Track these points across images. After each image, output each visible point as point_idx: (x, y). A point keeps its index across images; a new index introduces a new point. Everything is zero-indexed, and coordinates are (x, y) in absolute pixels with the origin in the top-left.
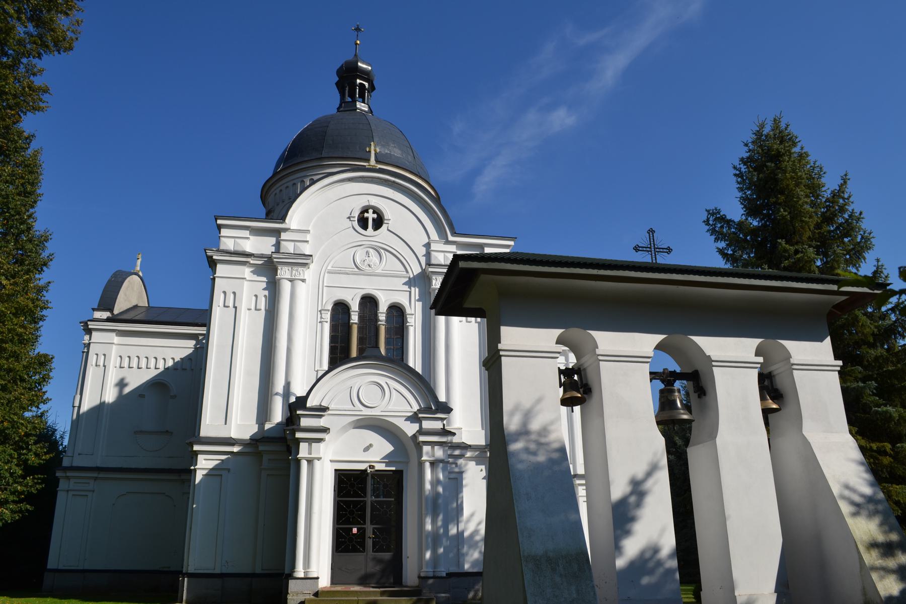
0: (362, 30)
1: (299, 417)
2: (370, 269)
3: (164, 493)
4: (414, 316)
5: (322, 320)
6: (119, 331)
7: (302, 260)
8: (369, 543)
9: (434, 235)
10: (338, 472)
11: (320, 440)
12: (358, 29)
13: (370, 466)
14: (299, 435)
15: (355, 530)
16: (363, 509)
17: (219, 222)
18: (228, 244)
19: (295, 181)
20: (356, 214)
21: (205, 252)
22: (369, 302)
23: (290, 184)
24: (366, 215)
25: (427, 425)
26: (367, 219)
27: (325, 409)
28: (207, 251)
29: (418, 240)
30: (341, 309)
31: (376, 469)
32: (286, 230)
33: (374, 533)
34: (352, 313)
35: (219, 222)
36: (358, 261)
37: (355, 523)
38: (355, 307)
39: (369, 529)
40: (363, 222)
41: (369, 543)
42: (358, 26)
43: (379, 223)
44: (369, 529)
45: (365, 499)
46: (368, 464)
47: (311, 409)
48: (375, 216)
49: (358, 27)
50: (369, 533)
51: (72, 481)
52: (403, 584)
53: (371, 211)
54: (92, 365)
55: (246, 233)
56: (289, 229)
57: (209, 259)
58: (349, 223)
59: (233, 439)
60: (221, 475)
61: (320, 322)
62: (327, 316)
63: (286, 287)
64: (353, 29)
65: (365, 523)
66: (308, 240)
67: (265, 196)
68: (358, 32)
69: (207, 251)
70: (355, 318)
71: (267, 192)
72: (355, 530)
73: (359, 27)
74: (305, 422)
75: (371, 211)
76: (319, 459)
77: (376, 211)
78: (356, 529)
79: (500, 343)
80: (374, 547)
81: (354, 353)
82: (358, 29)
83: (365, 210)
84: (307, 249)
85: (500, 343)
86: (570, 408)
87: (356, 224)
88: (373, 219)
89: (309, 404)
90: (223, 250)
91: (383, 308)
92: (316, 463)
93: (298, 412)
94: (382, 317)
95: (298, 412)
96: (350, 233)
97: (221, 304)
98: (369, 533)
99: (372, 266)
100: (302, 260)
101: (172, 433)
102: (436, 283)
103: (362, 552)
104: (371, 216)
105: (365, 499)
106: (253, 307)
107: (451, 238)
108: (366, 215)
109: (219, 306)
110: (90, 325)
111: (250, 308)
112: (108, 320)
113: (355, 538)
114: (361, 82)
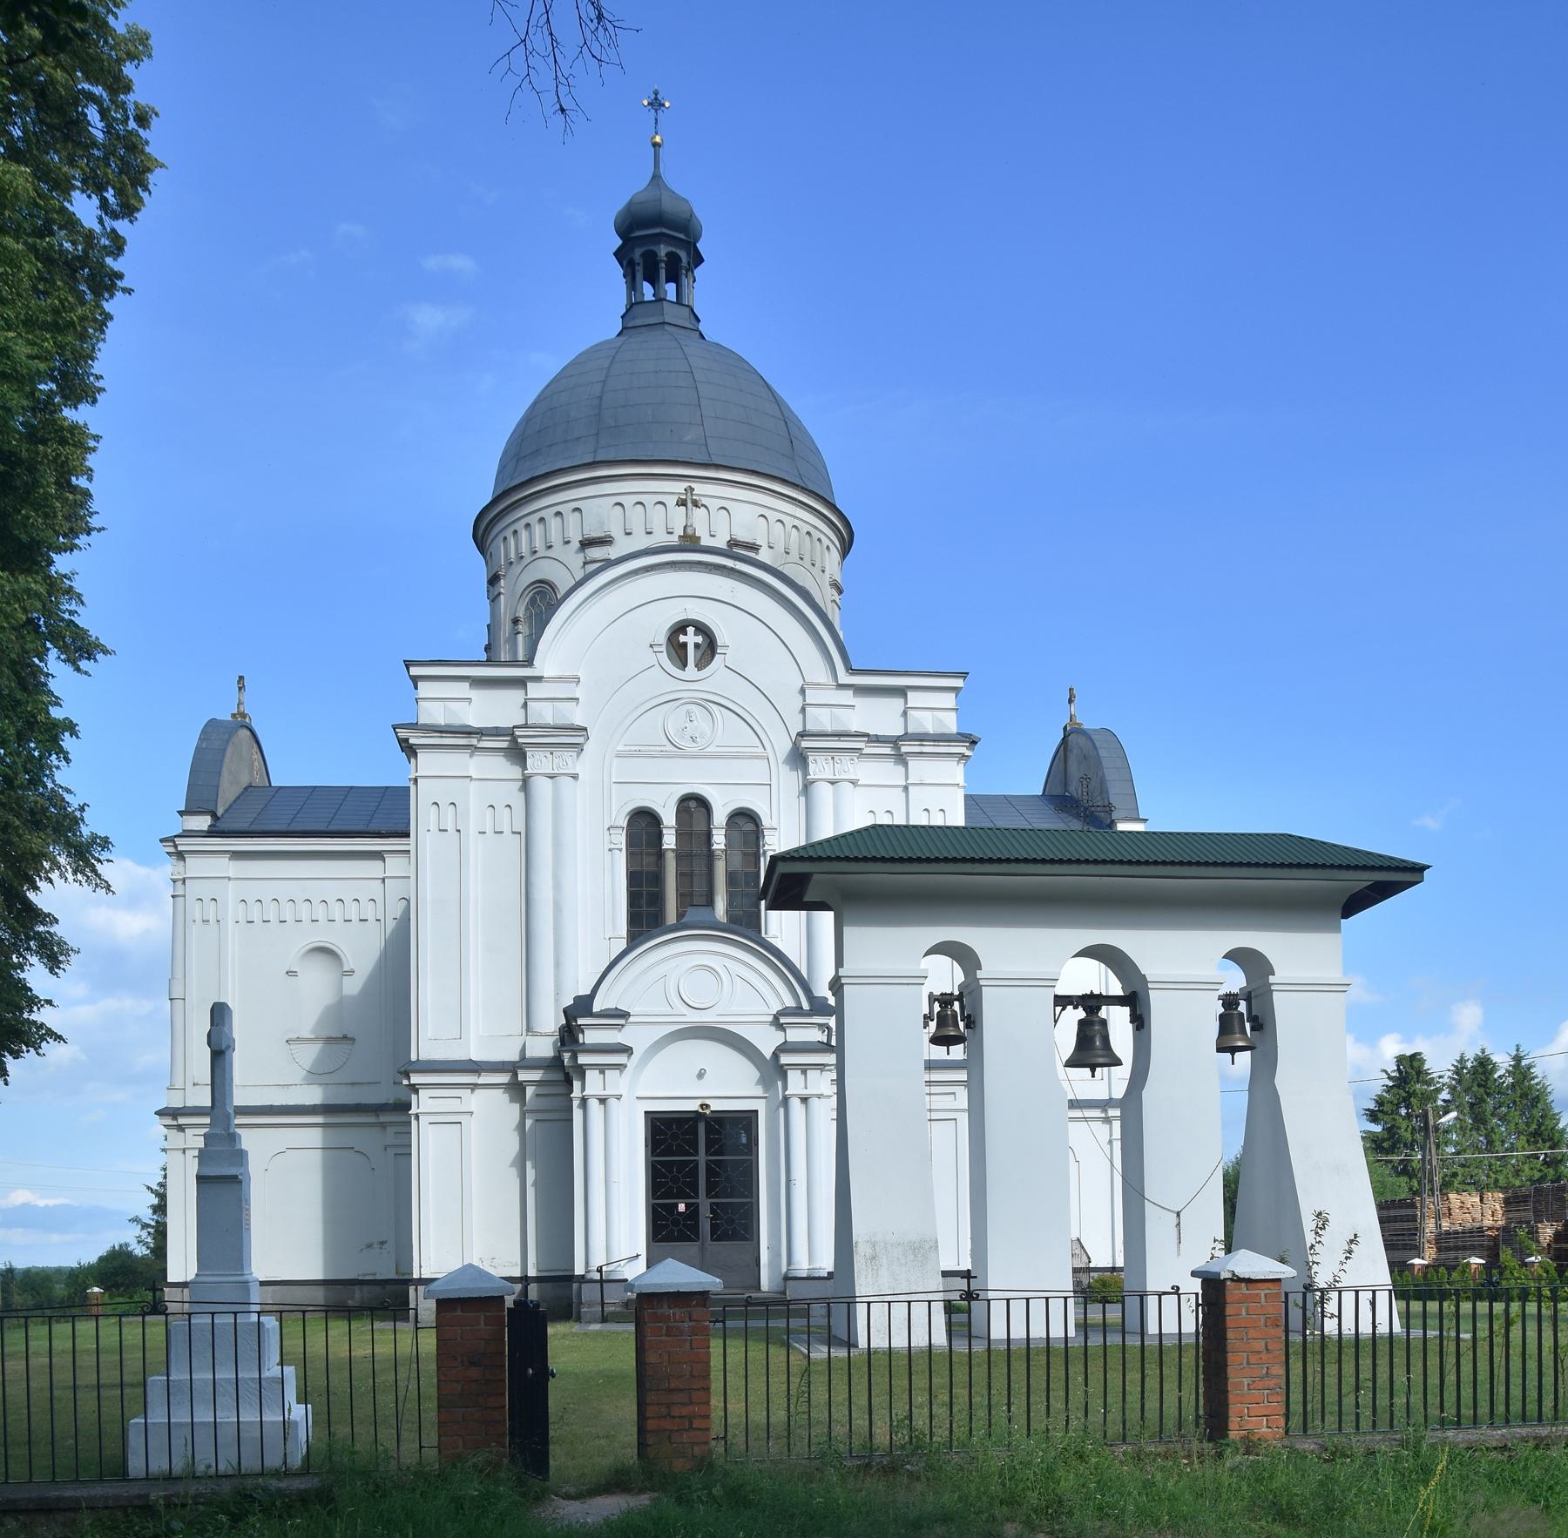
0: (667, 104)
1: (581, 1029)
2: (695, 745)
3: (353, 1148)
4: (776, 833)
5: (613, 846)
6: (234, 852)
7: (572, 737)
8: (705, 1226)
9: (816, 669)
10: (651, 1116)
11: (620, 1067)
12: (656, 104)
13: (702, 1106)
14: (583, 1059)
15: (682, 1207)
16: (694, 1172)
17: (415, 671)
18: (433, 714)
19: (542, 514)
20: (662, 639)
21: (396, 733)
22: (694, 807)
23: (533, 519)
24: (682, 638)
25: (794, 1035)
26: (685, 645)
27: (625, 1015)
28: (397, 730)
29: (783, 683)
30: (643, 823)
31: (712, 1109)
32: (538, 679)
33: (712, 1211)
34: (665, 831)
35: (415, 671)
36: (672, 733)
37: (682, 1195)
38: (669, 818)
39: (704, 1204)
40: (677, 651)
41: (705, 1226)
42: (656, 93)
43: (710, 648)
44: (704, 1204)
45: (695, 1158)
46: (699, 1102)
47: (601, 1015)
48: (699, 639)
49: (656, 99)
50: (705, 1212)
51: (391, 1130)
52: (762, 1288)
53: (691, 630)
54: (194, 921)
55: (463, 689)
56: (542, 677)
57: (403, 745)
58: (650, 658)
59: (474, 1062)
60: (955, 1119)
61: (610, 850)
62: (621, 839)
63: (542, 787)
64: (646, 103)
65: (697, 1196)
66: (577, 696)
67: (482, 544)
68: (656, 110)
69: (397, 730)
70: (669, 841)
71: (485, 530)
72: (682, 1207)
73: (660, 97)
74: (590, 1037)
75: (691, 630)
76: (619, 1097)
77: (702, 629)
78: (683, 1205)
79: (842, 967)
80: (713, 1232)
81: (671, 917)
82: (656, 104)
83: (681, 628)
84: (577, 717)
85: (842, 967)
86: (946, 1048)
87: (664, 658)
88: (697, 646)
89: (596, 1008)
90: (426, 725)
91: (720, 817)
92: (612, 1102)
93: (580, 1021)
94: (719, 841)
95: (580, 1021)
96: (661, 675)
97: (434, 828)
98: (705, 1212)
99: (698, 740)
100: (572, 737)
101: (353, 1040)
102: (814, 771)
103: (693, 1240)
104: (691, 638)
105: (695, 1158)
106: (489, 830)
107: (844, 678)
108: (682, 638)
109: (429, 831)
110: (180, 844)
111: (484, 830)
112: (212, 833)
113: (683, 1224)
114: (670, 249)
